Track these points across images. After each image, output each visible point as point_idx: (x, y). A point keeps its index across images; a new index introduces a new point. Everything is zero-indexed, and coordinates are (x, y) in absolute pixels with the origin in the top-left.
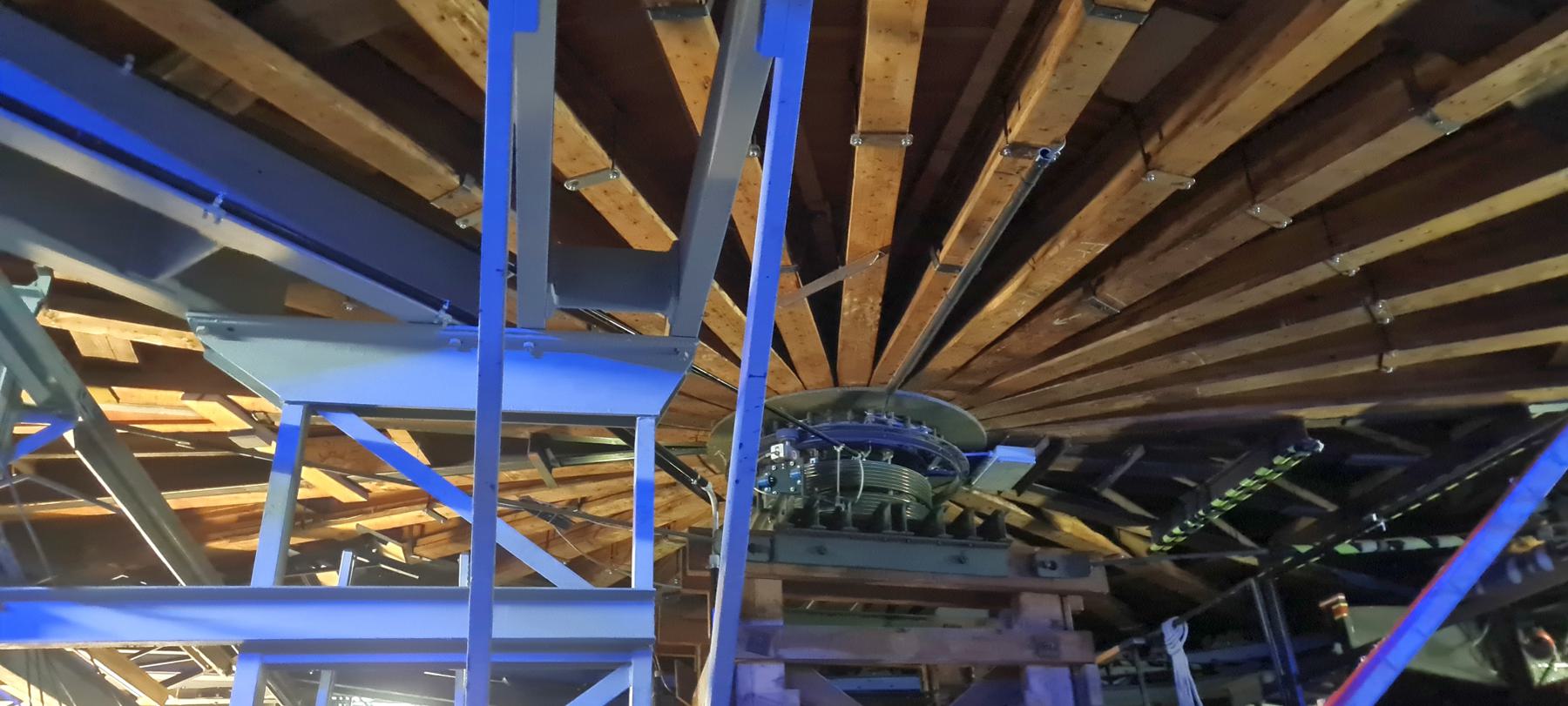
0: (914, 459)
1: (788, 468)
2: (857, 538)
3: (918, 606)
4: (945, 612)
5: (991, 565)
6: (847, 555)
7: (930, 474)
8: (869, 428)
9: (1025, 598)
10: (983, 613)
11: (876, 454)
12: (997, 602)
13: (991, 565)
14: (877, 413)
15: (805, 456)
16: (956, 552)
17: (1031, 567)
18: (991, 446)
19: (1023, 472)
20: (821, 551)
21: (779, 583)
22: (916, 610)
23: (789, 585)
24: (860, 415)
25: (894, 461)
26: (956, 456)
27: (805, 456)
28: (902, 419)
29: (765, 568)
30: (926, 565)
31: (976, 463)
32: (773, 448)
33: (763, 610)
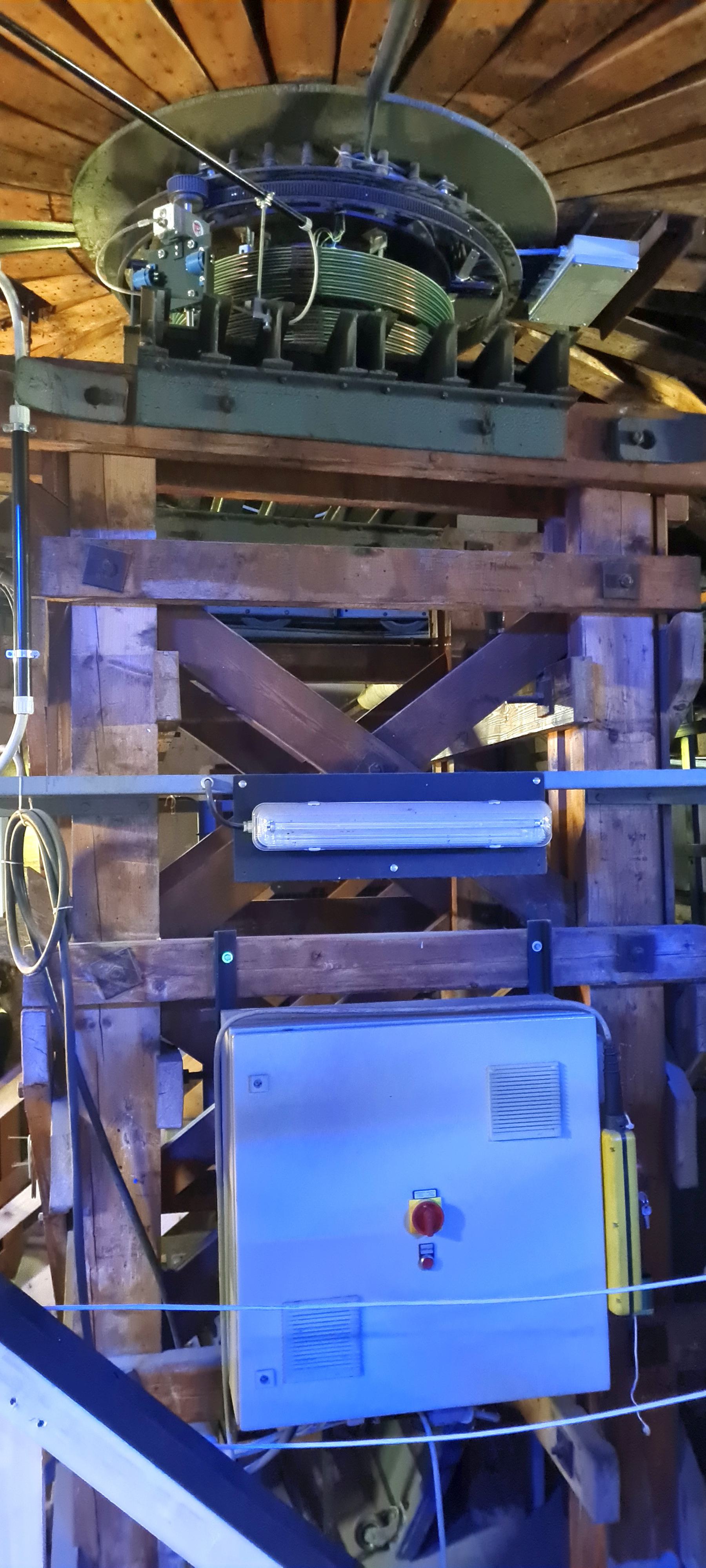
0: (435, 256)
1: (184, 252)
2: (292, 381)
3: (424, 509)
4: (471, 524)
5: (532, 438)
6: (272, 411)
7: (451, 287)
8: (340, 173)
9: (592, 498)
10: (529, 525)
11: (356, 239)
12: (547, 503)
13: (532, 438)
14: (357, 150)
15: (223, 241)
16: (472, 411)
17: (607, 440)
18: (564, 238)
19: (611, 288)
20: (225, 405)
21: (151, 464)
22: (424, 519)
23: (168, 469)
24: (325, 152)
25: (388, 253)
26: (500, 247)
27: (223, 241)
28: (404, 167)
29: (119, 434)
30: (422, 436)
31: (537, 270)
32: (157, 213)
33: (119, 511)
